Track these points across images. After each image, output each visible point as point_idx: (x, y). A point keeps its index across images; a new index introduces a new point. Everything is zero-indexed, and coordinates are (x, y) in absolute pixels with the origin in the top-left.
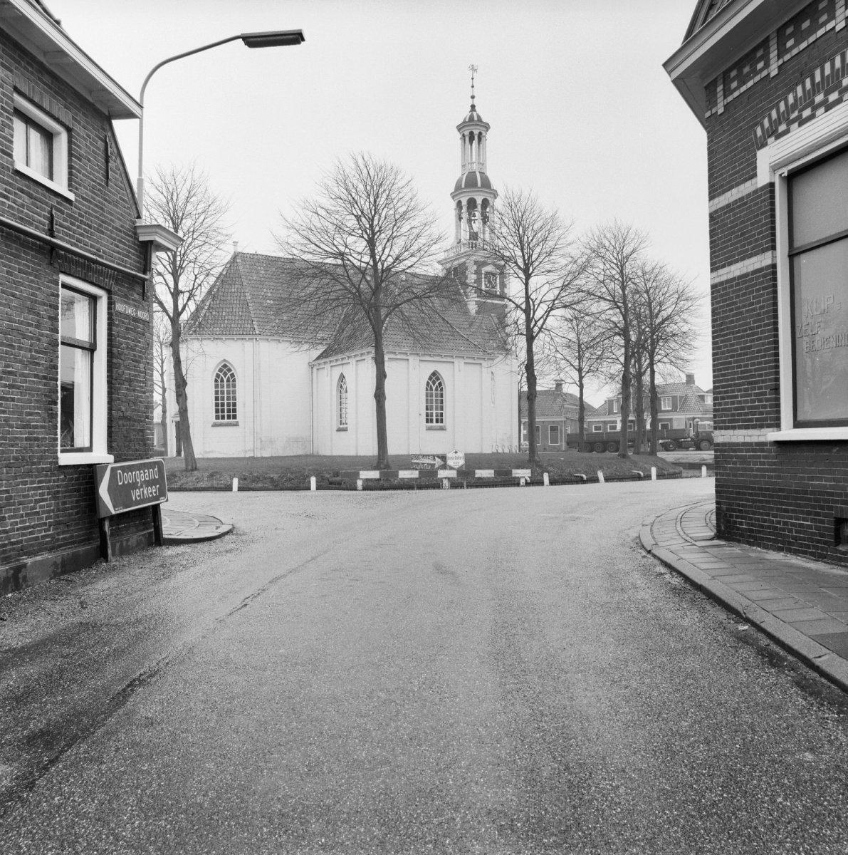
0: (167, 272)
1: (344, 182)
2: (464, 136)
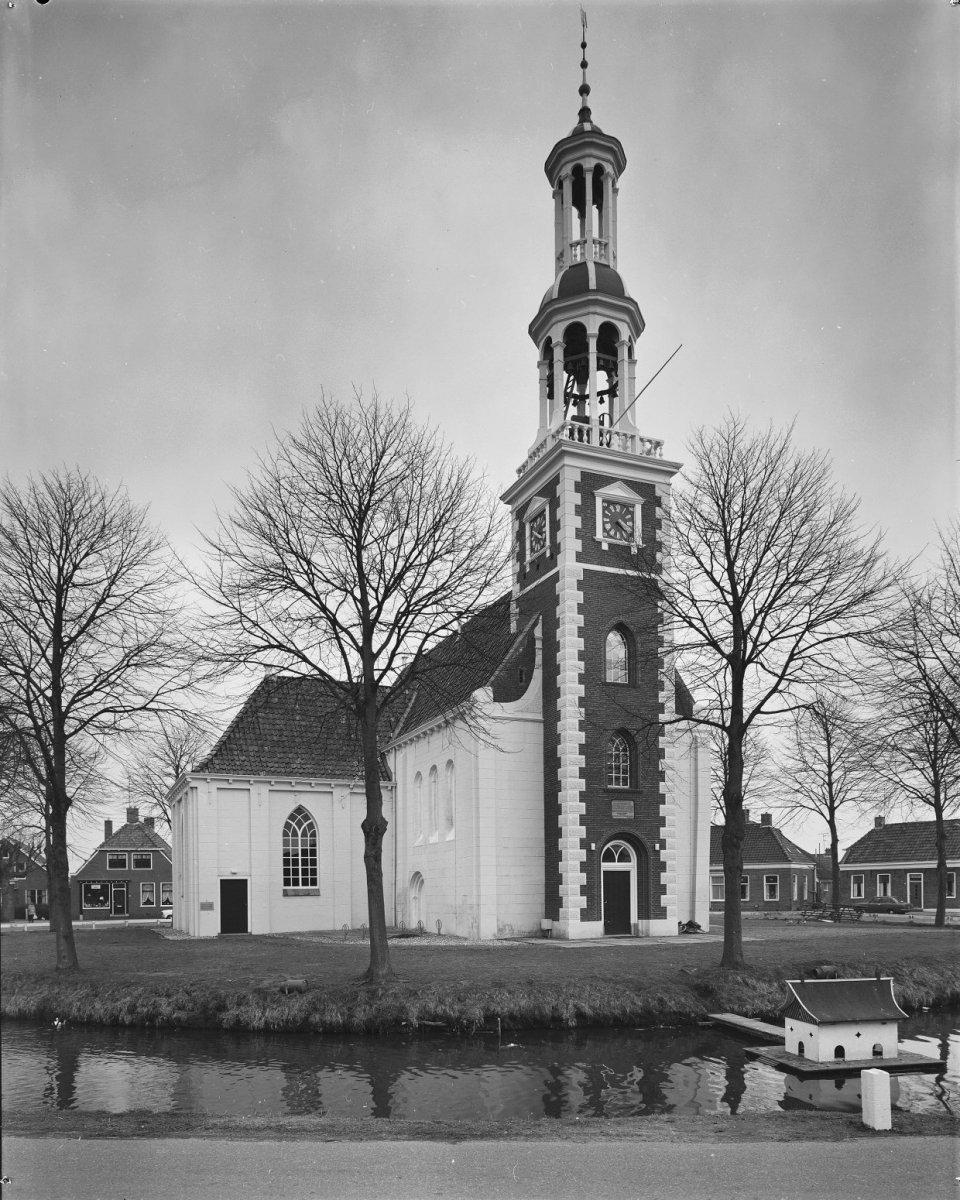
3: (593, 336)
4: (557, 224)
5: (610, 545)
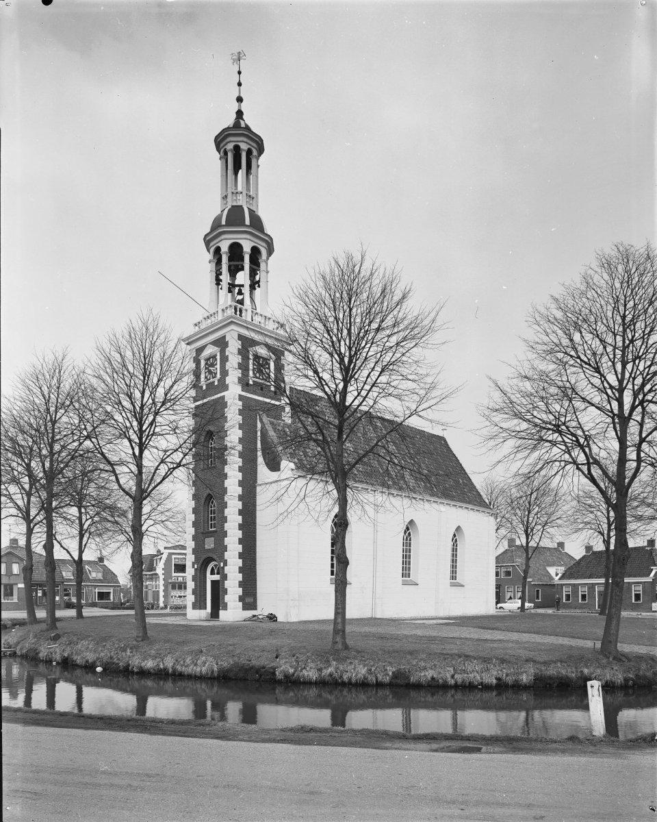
1: (58, 369)
5: (254, 381)
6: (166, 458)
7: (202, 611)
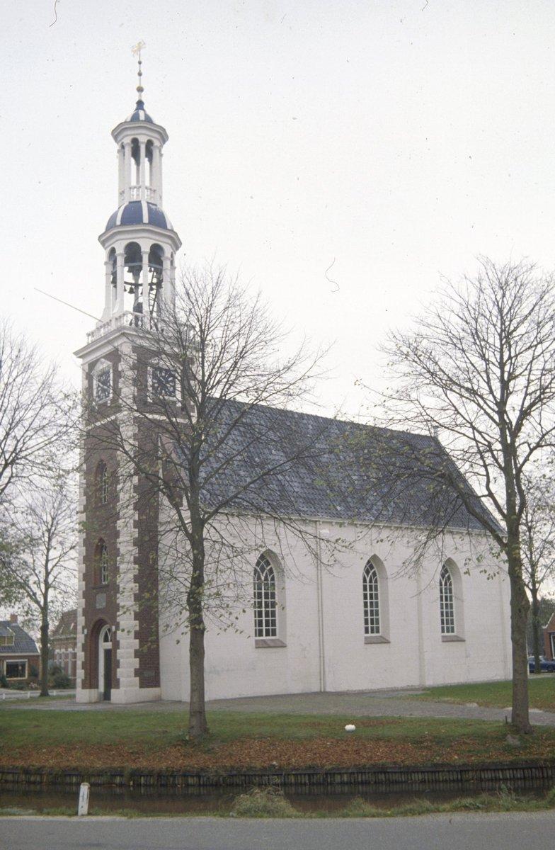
0: (40, 593)
2: (123, 147)
3: (145, 253)
4: (120, 170)
6: (494, 397)
7: (93, 690)
